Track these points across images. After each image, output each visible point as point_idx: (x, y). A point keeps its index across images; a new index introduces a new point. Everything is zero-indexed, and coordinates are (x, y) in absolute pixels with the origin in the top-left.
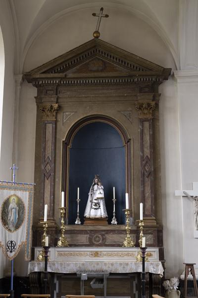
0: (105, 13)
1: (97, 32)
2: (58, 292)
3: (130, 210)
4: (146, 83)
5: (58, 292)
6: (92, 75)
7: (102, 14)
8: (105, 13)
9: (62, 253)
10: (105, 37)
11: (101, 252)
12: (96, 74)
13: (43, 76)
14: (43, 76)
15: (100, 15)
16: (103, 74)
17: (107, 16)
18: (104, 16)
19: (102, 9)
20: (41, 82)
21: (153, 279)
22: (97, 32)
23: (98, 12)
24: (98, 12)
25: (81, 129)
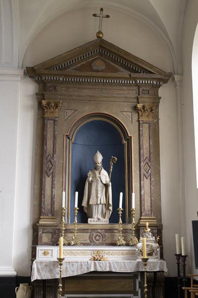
0: (105, 13)
1: (100, 32)
2: (137, 280)
3: (75, 216)
4: (157, 80)
5: (137, 280)
6: (95, 74)
7: (101, 14)
8: (105, 13)
9: (74, 252)
10: (106, 37)
11: (102, 250)
12: (100, 74)
13: (78, 73)
14: (78, 73)
15: (101, 16)
16: (109, 75)
17: (108, 16)
18: (105, 16)
19: (102, 10)
20: (51, 80)
21: (157, 277)
22: (100, 32)
23: (98, 12)
24: (98, 12)
25: (110, 124)
